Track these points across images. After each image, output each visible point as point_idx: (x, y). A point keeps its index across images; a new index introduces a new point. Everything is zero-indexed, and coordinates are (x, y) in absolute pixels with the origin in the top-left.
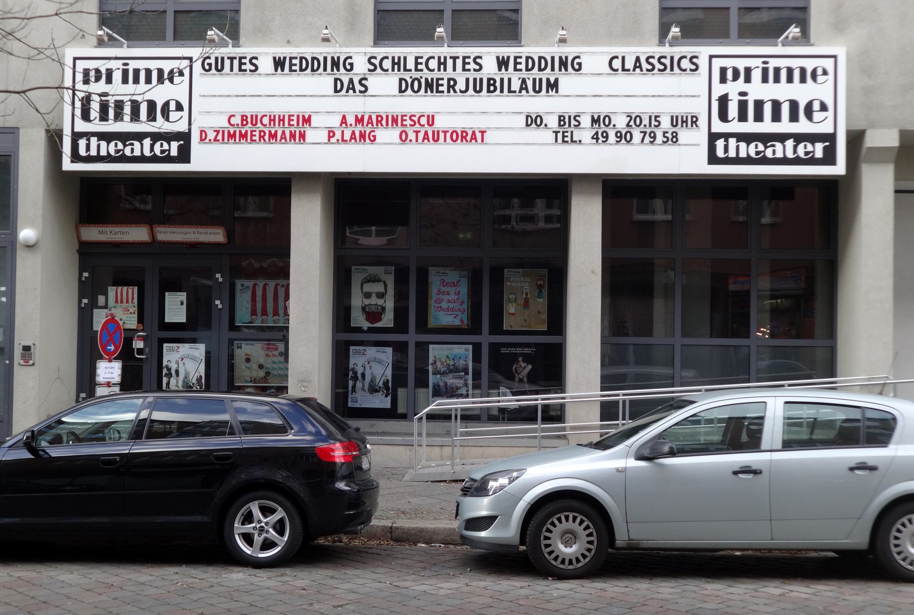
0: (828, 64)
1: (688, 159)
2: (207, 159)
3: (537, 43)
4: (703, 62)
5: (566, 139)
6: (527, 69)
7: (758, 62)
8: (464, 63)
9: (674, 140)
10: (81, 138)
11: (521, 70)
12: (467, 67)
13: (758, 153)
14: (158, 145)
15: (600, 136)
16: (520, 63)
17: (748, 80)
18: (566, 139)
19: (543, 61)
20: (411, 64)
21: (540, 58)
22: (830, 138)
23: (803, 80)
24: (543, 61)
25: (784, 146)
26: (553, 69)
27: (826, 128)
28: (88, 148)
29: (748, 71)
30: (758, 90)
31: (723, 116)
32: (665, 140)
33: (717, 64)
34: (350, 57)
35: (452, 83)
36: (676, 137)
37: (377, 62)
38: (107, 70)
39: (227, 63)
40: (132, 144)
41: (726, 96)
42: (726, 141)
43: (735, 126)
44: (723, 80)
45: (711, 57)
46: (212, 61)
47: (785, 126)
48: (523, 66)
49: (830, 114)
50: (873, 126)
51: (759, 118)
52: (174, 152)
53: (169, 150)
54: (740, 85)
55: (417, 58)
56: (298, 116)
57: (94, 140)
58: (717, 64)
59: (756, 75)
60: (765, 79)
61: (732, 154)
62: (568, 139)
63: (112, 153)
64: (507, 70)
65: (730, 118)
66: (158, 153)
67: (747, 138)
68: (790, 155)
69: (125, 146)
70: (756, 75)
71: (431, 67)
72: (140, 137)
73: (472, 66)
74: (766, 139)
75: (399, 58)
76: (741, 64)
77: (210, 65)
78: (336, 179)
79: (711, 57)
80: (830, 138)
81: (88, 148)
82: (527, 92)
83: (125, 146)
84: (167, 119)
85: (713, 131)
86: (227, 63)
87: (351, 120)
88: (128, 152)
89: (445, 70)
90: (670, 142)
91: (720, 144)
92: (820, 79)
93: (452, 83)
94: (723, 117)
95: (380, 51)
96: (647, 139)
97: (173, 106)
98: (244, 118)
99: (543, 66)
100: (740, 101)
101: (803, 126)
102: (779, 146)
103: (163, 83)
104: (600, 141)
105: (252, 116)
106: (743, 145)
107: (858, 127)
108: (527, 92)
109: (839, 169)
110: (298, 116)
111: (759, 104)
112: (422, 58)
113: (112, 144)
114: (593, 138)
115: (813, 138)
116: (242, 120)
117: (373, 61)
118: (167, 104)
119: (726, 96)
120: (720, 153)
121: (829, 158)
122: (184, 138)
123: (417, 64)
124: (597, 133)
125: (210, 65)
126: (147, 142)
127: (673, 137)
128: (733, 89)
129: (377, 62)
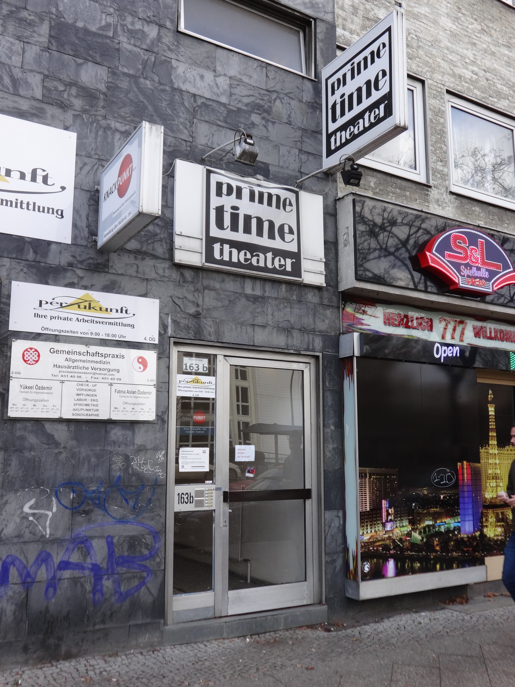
10: (217, 242)
14: (277, 259)
40: (258, 255)
41: (223, 207)
43: (227, 234)
44: (219, 193)
57: (226, 247)
63: (242, 261)
65: (225, 227)
81: (222, 253)
88: (254, 261)
94: (220, 225)
111: (248, 218)
113: (242, 253)
118: (282, 227)
119: (223, 207)
128: (228, 202)
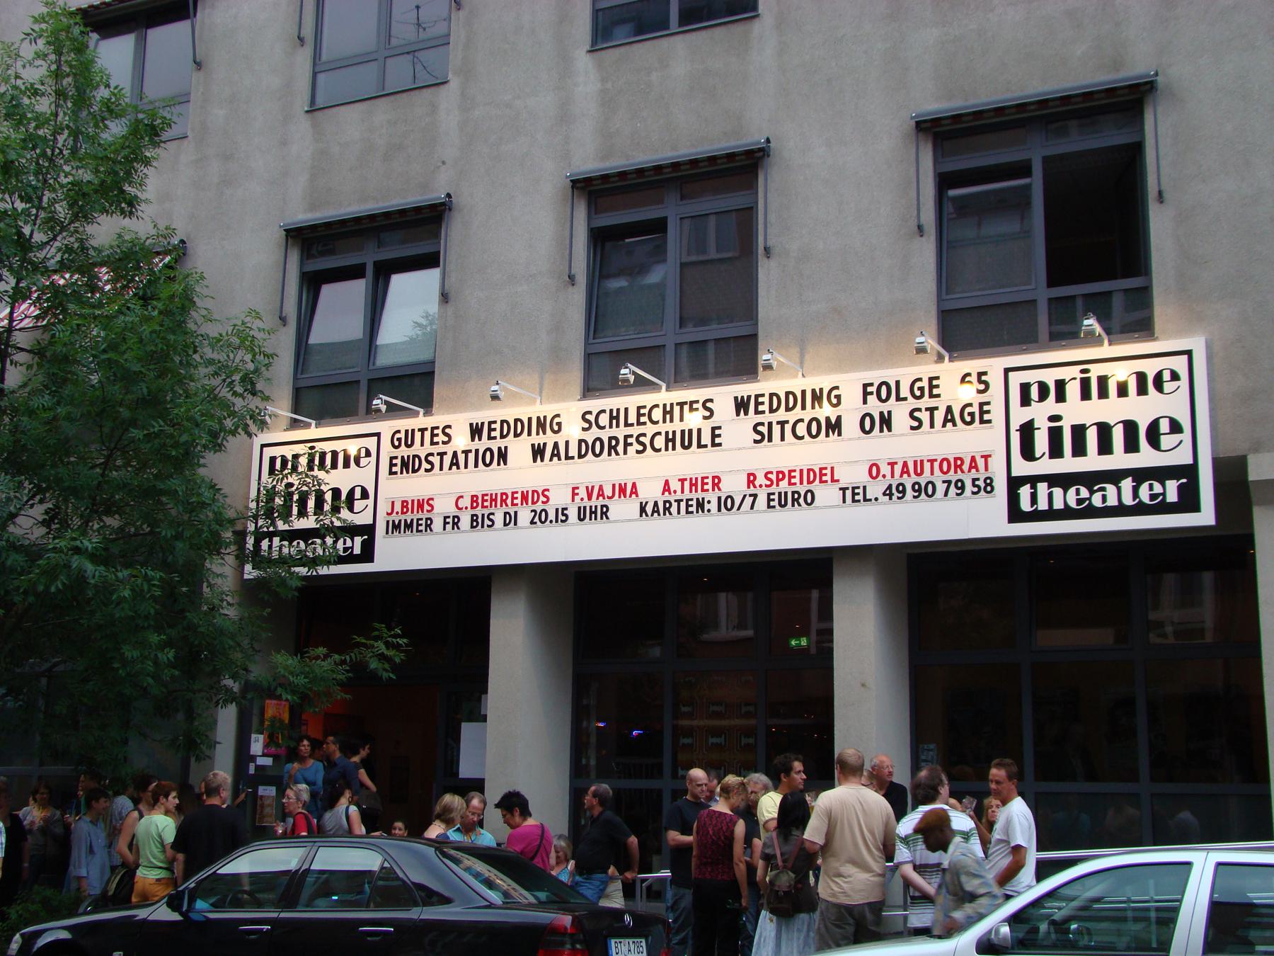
0: (1180, 364)
1: (983, 519)
2: (394, 554)
3: (789, 373)
4: (996, 380)
5: (857, 498)
6: (772, 411)
7: (1075, 371)
8: (433, 435)
9: (989, 489)
11: (763, 412)
12: (436, 439)
13: (1079, 502)
15: (894, 490)
16: (762, 403)
17: (1061, 398)
18: (857, 498)
19: (791, 397)
20: (632, 418)
21: (787, 394)
22: (1188, 473)
23: (346, 465)
24: (791, 397)
25: (1119, 489)
26: (803, 408)
27: (1182, 457)
28: (1034, 499)
29: (1060, 385)
30: (1075, 411)
31: (1028, 453)
32: (976, 490)
33: (1016, 379)
34: (837, 388)
35: (614, 443)
36: (990, 484)
37: (591, 418)
38: (1057, 382)
39: (418, 435)
40: (1103, 489)
41: (1031, 422)
42: (1034, 487)
43: (1046, 466)
44: (1025, 401)
45: (1007, 371)
46: (402, 435)
47: (1119, 459)
48: (765, 407)
49: (1186, 435)
50: (1257, 448)
51: (1079, 450)
52: (1172, 497)
53: (1164, 494)
54: (1051, 407)
55: (639, 408)
56: (801, 471)
58: (1016, 379)
59: (1073, 390)
60: (1085, 395)
61: (1043, 505)
62: (860, 497)
63: (1072, 504)
64: (480, 439)
66: (1146, 500)
67: (1063, 481)
68: (1128, 500)
69: (1092, 492)
70: (1073, 390)
71: (655, 419)
72: (1114, 477)
73: (442, 438)
74: (1092, 480)
75: (618, 410)
76: (1050, 377)
77: (921, 389)
78: (909, 556)
79: (1007, 371)
80: (1188, 473)
81: (1034, 499)
82: (955, 425)
83: (1092, 492)
84: (351, 509)
85: (1014, 474)
86: (418, 435)
87: (675, 485)
88: (1097, 500)
89: (672, 421)
90: (982, 492)
91: (1025, 491)
92: (1168, 387)
93: (614, 443)
95: (595, 405)
96: (953, 490)
97: (358, 494)
98: (474, 499)
99: (791, 405)
100: (1050, 429)
101: (1146, 457)
102: (1111, 489)
103: (1029, 405)
104: (894, 498)
105: (915, 462)
106: (1058, 492)
107: (1229, 451)
108: (955, 425)
109: (1206, 516)
110: (801, 471)
112: (871, 385)
114: (884, 494)
115: (1161, 474)
116: (472, 501)
117: (588, 417)
118: (352, 492)
119: (1031, 422)
120: (1025, 505)
121: (1189, 501)
122: (369, 530)
123: (639, 415)
124: (890, 487)
125: (399, 440)
126: (1127, 484)
127: (987, 485)
128: (1040, 413)
129: (591, 418)
